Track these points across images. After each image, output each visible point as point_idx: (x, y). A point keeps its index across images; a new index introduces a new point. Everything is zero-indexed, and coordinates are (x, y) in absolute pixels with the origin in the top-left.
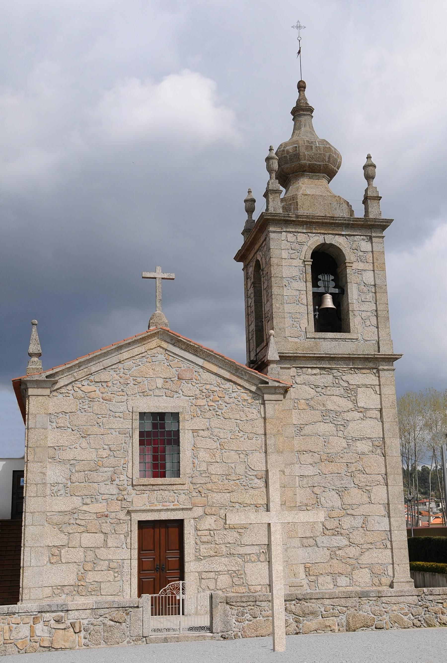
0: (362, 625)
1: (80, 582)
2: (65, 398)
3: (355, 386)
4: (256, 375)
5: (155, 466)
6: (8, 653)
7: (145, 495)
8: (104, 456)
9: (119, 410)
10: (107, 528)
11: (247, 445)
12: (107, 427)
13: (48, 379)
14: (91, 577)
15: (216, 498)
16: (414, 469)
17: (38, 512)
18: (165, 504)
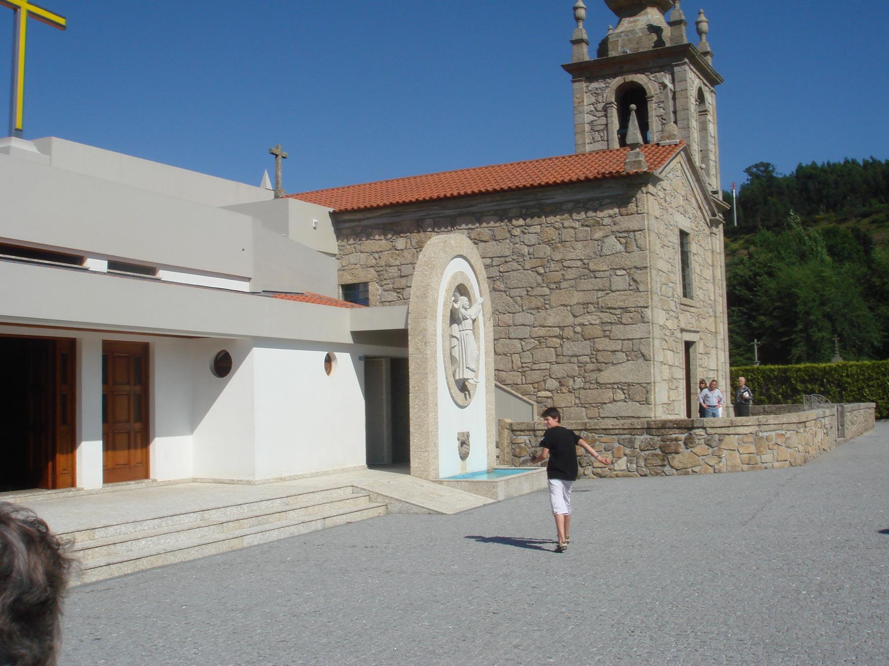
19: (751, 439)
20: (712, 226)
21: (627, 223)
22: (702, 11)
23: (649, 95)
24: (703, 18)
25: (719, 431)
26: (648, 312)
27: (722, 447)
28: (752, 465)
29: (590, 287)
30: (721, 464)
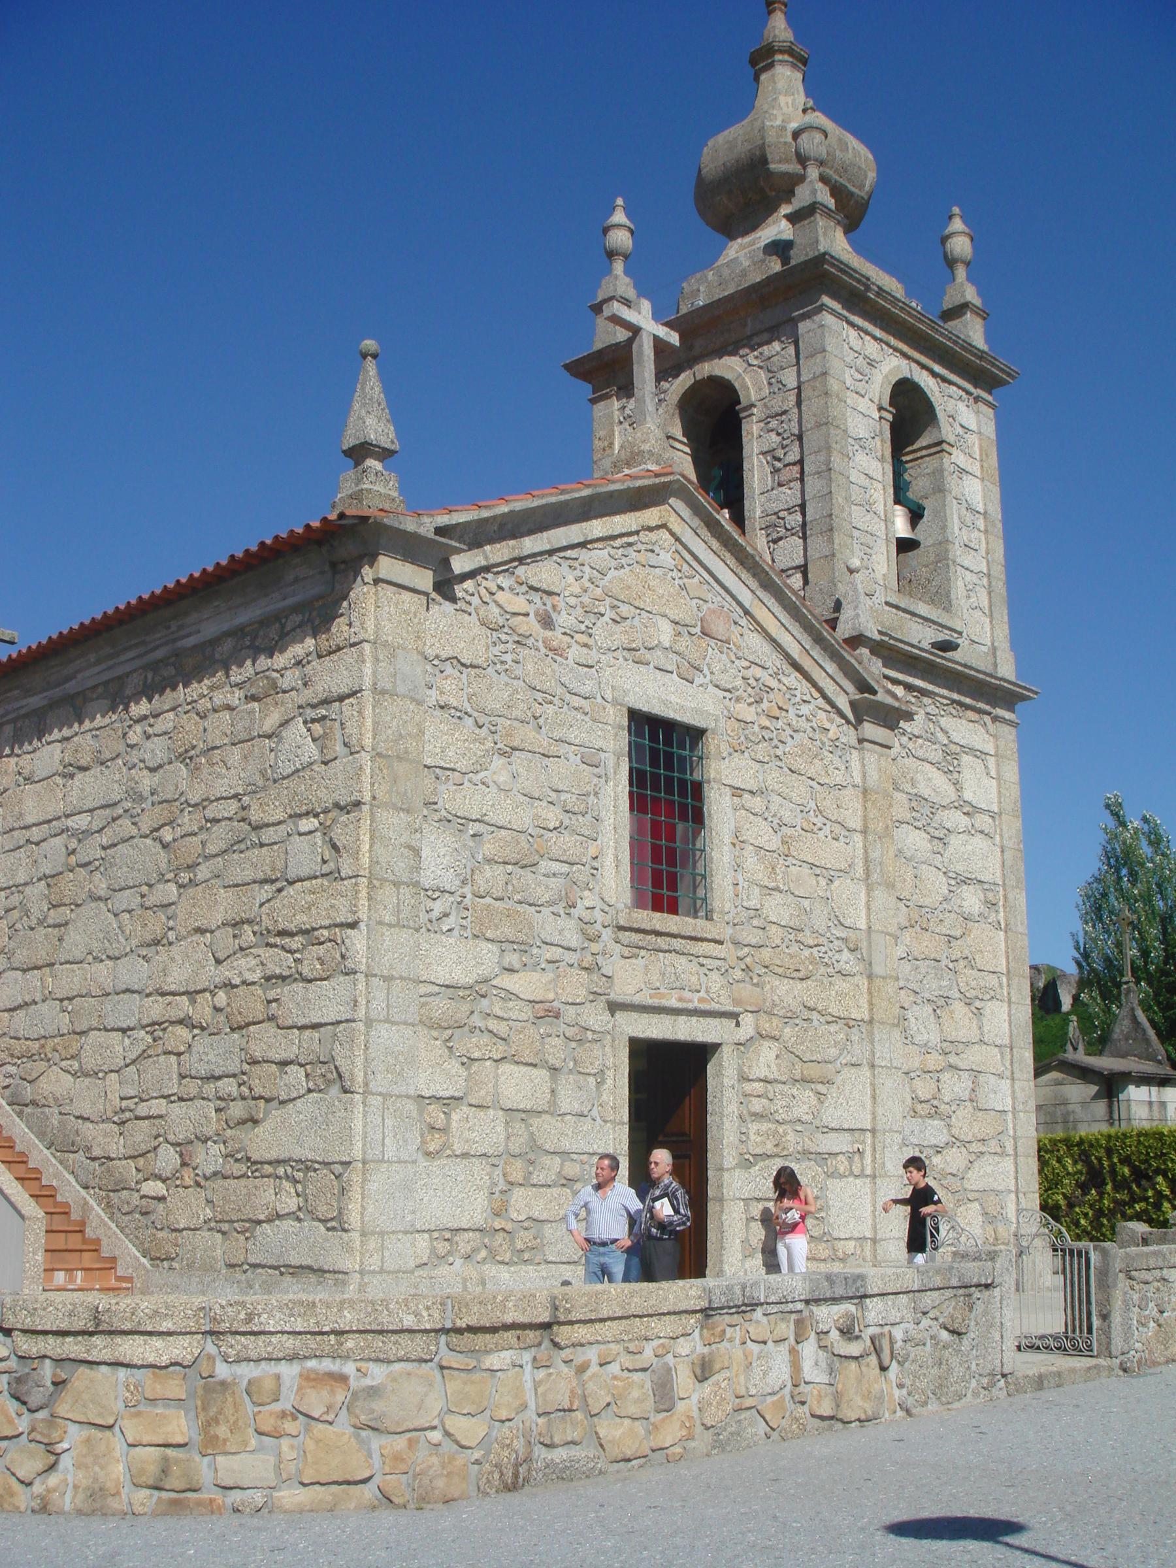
1: (498, 1220)
2: (460, 615)
3: (958, 749)
4: (856, 665)
6: (744, 1444)
7: (640, 961)
8: (551, 827)
10: (556, 1050)
11: (831, 853)
12: (556, 735)
13: (437, 538)
14: (522, 1204)
16: (1093, 970)
17: (401, 978)
19: (175, 1387)
20: (860, 721)
21: (331, 677)
22: (956, 210)
23: (744, 402)
24: (957, 225)
25: (51, 1345)
26: (357, 941)
27: (62, 1409)
28: (175, 1495)
29: (248, 874)
30: (53, 1480)
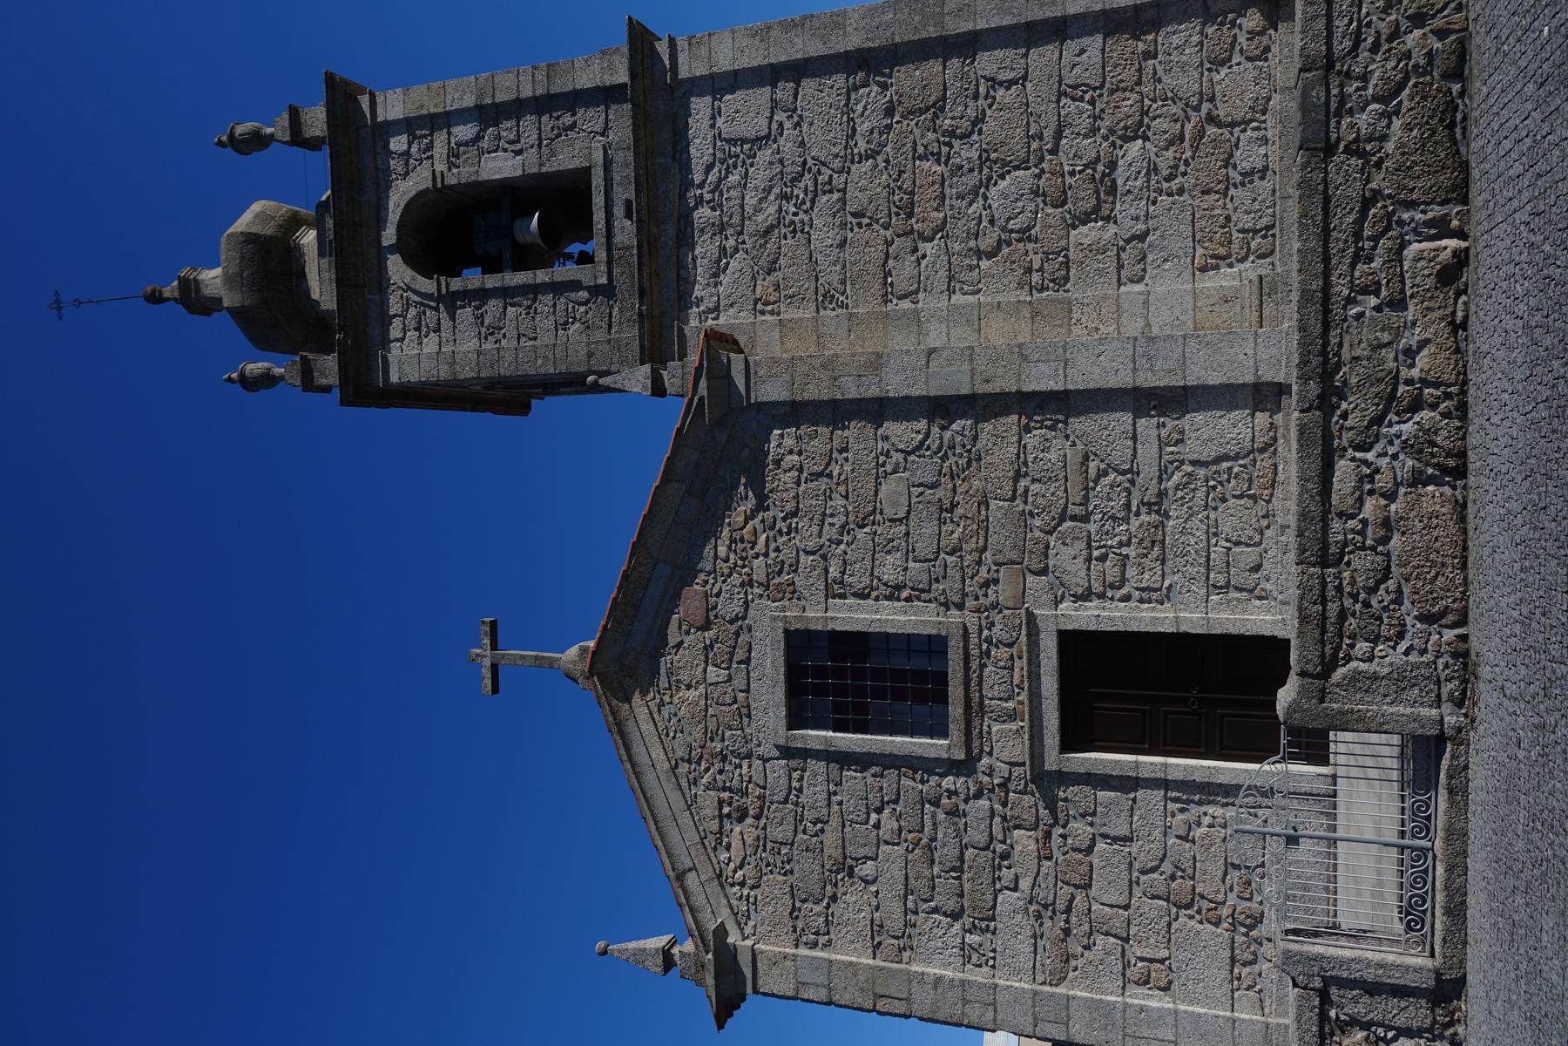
0: (1442, 134)
5: (920, 698)
9: (784, 781)
12: (825, 811)
15: (1001, 538)
18: (1016, 681)
